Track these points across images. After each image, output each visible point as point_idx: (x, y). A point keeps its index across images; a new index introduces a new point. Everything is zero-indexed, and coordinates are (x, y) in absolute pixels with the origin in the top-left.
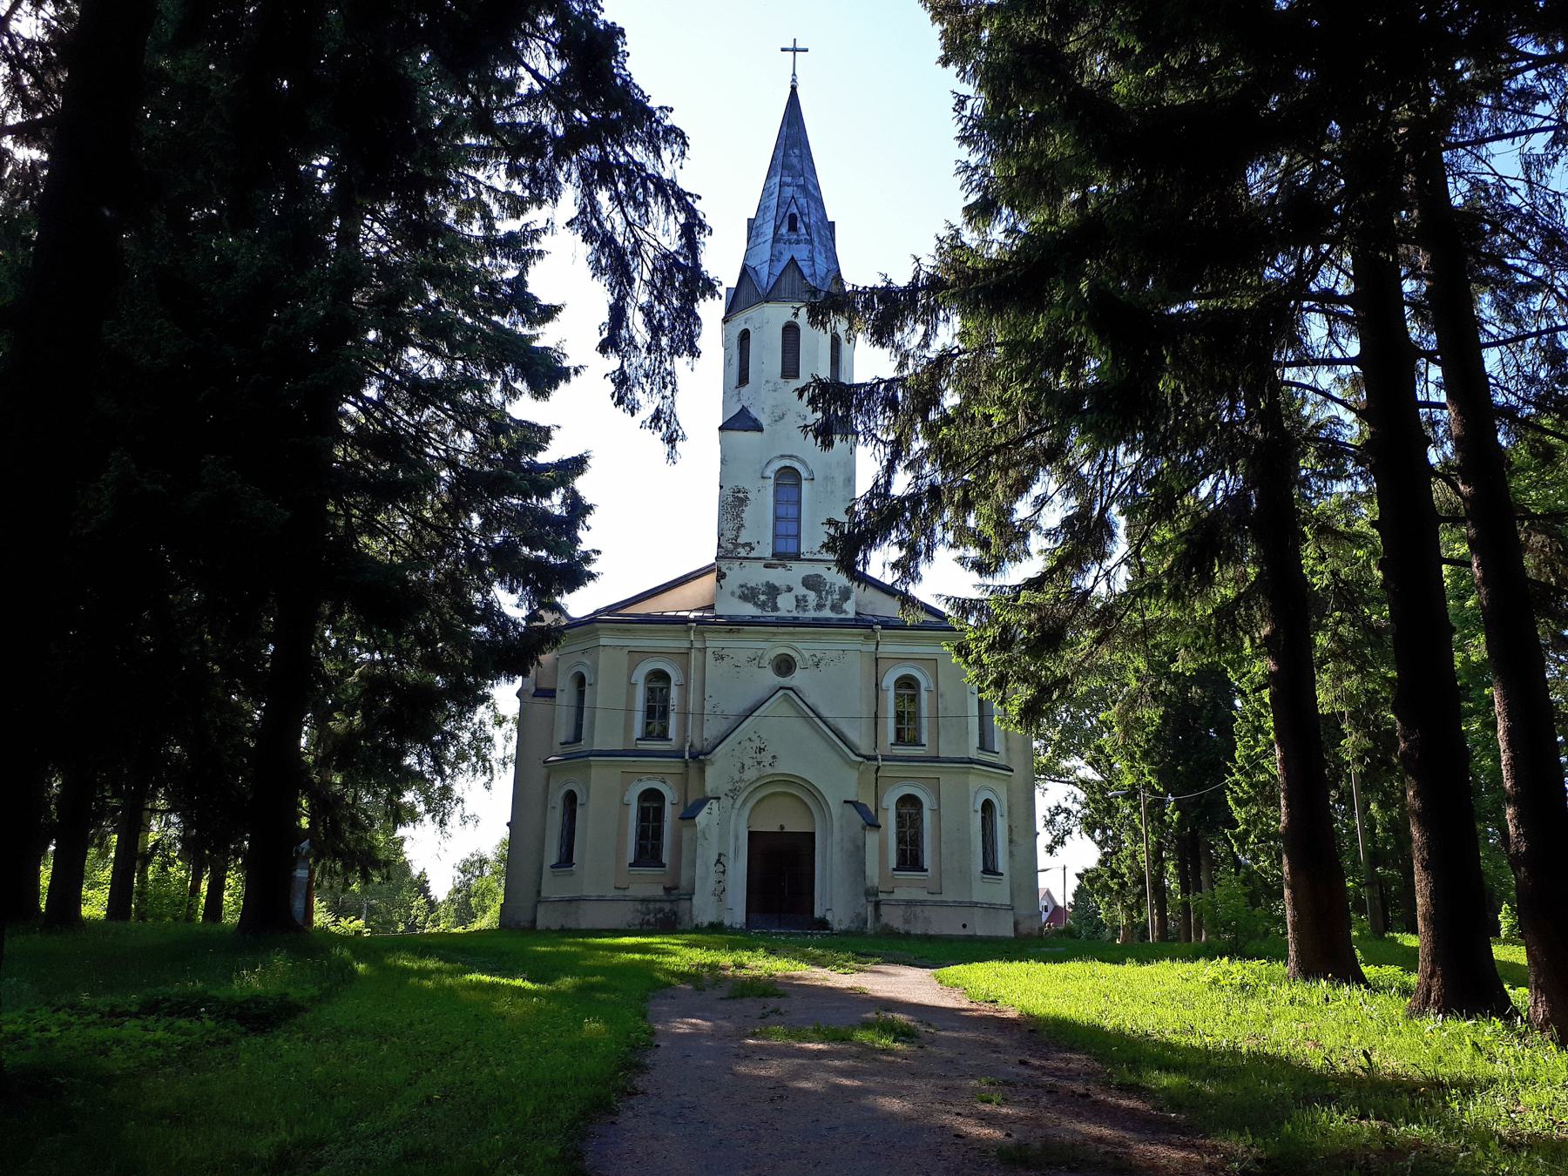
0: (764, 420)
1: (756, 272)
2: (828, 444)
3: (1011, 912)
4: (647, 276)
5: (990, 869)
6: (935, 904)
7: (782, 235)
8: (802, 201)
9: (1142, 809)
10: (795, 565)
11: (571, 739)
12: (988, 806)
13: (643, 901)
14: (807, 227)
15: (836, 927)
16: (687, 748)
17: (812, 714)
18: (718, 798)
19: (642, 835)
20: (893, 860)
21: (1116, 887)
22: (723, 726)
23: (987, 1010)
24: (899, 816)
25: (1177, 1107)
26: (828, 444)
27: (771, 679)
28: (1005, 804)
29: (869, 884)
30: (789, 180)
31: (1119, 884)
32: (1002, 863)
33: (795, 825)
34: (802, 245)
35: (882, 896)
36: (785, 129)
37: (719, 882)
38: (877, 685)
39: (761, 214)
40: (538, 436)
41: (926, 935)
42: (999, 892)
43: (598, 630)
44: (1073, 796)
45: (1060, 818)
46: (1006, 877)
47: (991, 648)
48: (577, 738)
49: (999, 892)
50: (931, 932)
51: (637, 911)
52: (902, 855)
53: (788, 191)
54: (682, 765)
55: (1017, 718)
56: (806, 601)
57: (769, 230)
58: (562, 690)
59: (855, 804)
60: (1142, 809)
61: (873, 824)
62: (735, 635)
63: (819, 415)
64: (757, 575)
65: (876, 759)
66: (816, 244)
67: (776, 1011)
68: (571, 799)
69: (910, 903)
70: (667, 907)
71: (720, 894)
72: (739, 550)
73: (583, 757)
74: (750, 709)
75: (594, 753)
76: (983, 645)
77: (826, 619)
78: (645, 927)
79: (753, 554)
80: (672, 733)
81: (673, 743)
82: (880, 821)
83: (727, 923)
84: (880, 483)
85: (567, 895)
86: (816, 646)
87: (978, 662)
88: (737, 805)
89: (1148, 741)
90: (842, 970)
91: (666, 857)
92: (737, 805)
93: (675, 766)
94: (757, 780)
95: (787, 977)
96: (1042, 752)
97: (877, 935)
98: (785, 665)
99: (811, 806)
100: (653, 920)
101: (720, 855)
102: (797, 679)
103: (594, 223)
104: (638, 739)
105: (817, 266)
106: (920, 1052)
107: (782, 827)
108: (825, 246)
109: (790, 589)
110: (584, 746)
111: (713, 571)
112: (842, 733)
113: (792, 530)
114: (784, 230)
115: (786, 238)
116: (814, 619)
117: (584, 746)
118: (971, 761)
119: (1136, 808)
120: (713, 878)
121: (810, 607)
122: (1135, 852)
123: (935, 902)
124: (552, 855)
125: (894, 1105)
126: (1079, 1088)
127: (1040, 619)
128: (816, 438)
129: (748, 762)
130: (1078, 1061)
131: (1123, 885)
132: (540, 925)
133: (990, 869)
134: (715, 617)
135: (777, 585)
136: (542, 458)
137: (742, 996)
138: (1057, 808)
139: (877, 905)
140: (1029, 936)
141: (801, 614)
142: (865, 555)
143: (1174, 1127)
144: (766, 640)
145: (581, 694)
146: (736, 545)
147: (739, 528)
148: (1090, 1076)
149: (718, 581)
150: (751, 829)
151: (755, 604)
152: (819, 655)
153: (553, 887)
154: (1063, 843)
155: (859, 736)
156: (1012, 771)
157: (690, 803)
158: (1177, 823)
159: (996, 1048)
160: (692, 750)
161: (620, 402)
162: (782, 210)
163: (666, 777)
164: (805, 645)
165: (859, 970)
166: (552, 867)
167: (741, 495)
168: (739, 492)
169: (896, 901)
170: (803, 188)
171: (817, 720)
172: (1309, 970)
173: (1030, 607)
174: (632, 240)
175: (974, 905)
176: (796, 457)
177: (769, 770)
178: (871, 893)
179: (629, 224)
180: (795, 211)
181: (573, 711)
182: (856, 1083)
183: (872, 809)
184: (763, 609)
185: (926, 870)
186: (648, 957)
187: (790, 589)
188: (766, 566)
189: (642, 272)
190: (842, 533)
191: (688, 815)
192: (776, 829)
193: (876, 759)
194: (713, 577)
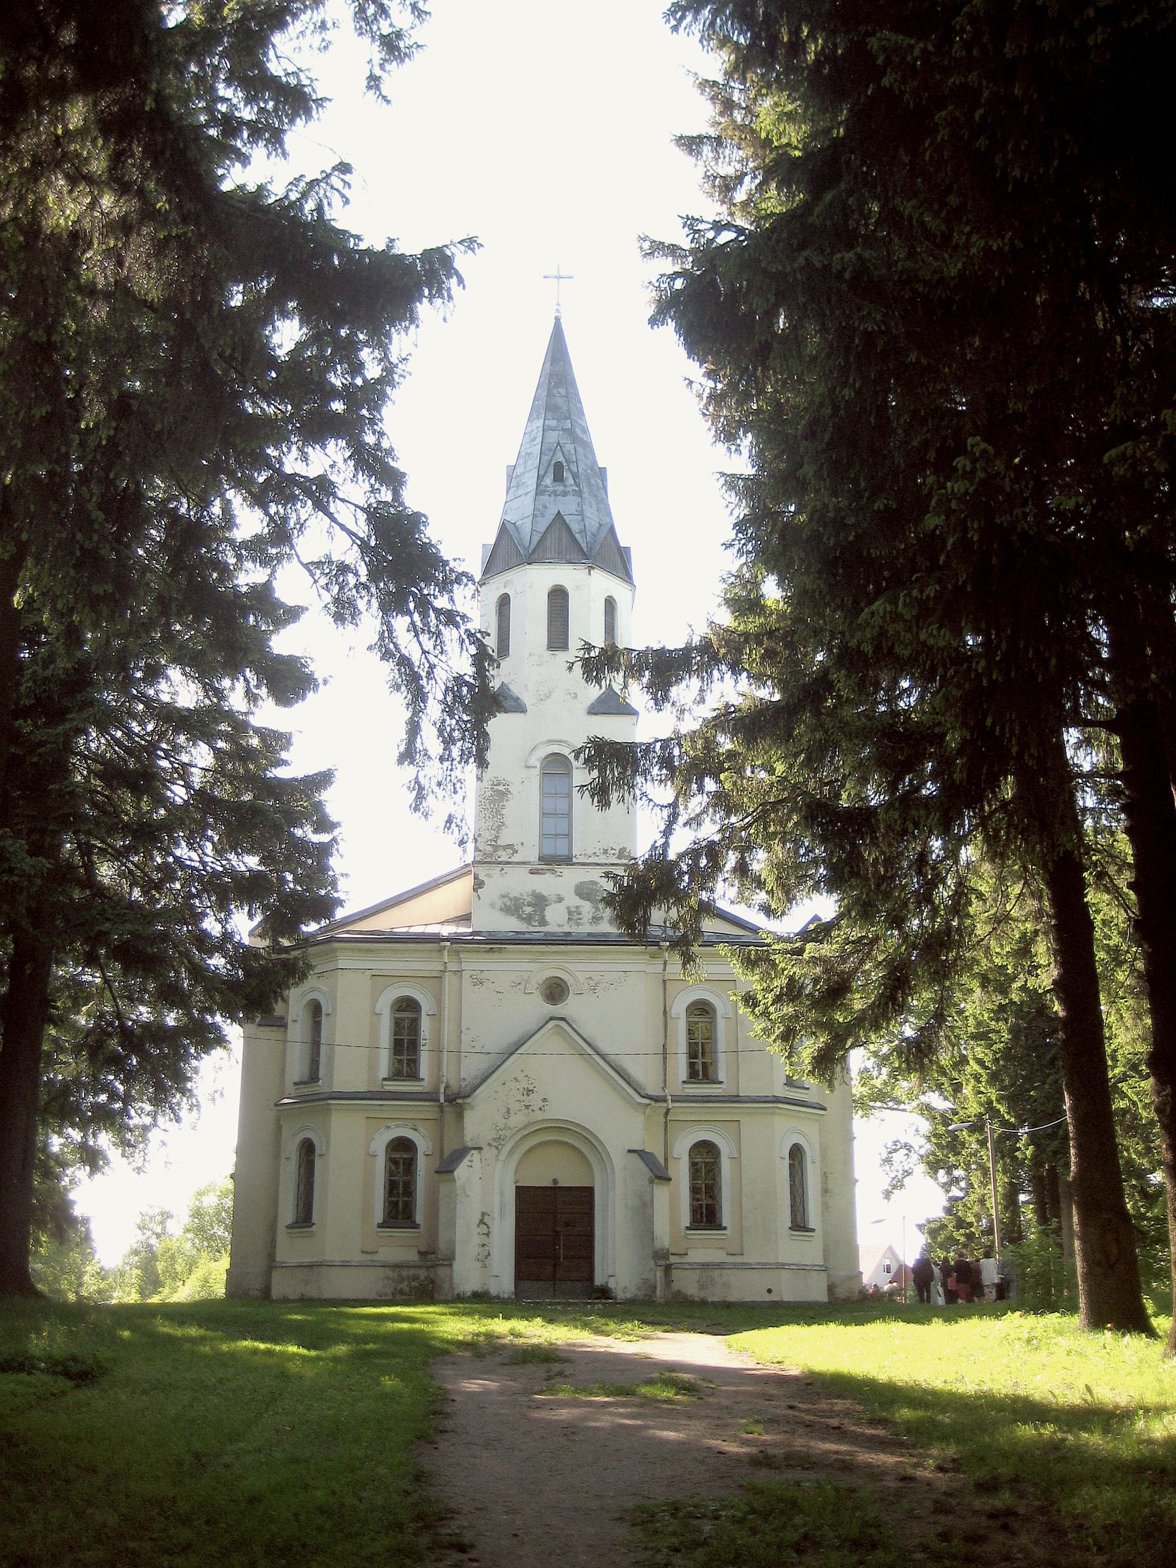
0: (527, 699)
1: (516, 528)
2: (605, 803)
3: (824, 1274)
4: (441, 697)
5: (799, 1225)
6: (736, 1266)
7: (547, 486)
8: (569, 447)
9: (989, 1145)
10: (566, 871)
11: (305, 1079)
12: (796, 1153)
13: (397, 1266)
14: (575, 476)
15: (620, 1295)
16: (442, 1090)
17: (590, 1051)
18: (479, 1149)
19: (391, 1187)
20: (686, 1218)
21: (962, 1239)
22: (483, 1063)
23: (773, 1369)
24: (693, 1165)
25: (909, 1431)
26: (605, 803)
27: (540, 1007)
28: (817, 1147)
29: (658, 1244)
30: (553, 423)
31: (966, 1235)
32: (814, 1220)
33: (570, 1178)
34: (570, 498)
35: (673, 1259)
36: (548, 365)
37: (484, 1245)
38: (665, 1012)
39: (522, 461)
40: (275, 741)
41: (725, 1302)
42: (808, 1251)
43: (335, 950)
44: (914, 1128)
45: (899, 1156)
46: (818, 1233)
47: (778, 1000)
48: (314, 1077)
49: (808, 1251)
50: (731, 1299)
51: (388, 1278)
52: (695, 1211)
53: (553, 437)
54: (438, 1109)
55: (809, 1068)
56: (580, 914)
57: (531, 481)
58: (295, 1021)
59: (641, 1154)
60: (989, 1145)
61: (661, 1176)
62: (496, 955)
63: (595, 773)
64: (521, 883)
65: (665, 1101)
66: (586, 495)
67: (560, 1374)
68: (308, 1148)
69: (705, 1266)
70: (422, 1273)
71: (484, 1259)
72: (499, 853)
73: (324, 1099)
74: (515, 1043)
75: (334, 1095)
76: (770, 997)
77: (604, 934)
78: (398, 1297)
79: (515, 859)
80: (424, 1070)
81: (424, 1083)
82: (671, 1173)
83: (493, 1292)
84: (657, 844)
85: (306, 1260)
86: (591, 967)
87: (766, 1014)
88: (503, 1156)
89: (996, 1061)
90: (626, 1338)
91: (419, 1217)
92: (503, 1156)
93: (427, 1110)
94: (525, 1127)
95: (568, 1345)
96: (875, 1073)
97: (667, 1303)
98: (555, 991)
99: (583, 1150)
100: (407, 1289)
101: (483, 1214)
102: (570, 1007)
103: (391, 646)
104: (384, 1079)
105: (587, 521)
106: (699, 1402)
107: (555, 1181)
108: (595, 496)
109: (560, 899)
110: (322, 1086)
111: (468, 873)
112: (624, 1070)
113: (562, 828)
114: (548, 481)
115: (551, 489)
116: (589, 934)
117: (322, 1086)
118: (777, 1100)
119: (982, 1143)
120: (477, 1240)
121: (585, 920)
122: (984, 1196)
123: (735, 1264)
124: (287, 1213)
125: (670, 1435)
126: (834, 1422)
127: (826, 971)
128: (592, 797)
129: (515, 1106)
130: (840, 1404)
131: (970, 1237)
132: (276, 1292)
133: (799, 1225)
134: (472, 934)
135: (545, 894)
136: (281, 773)
137: (525, 1362)
138: (895, 1143)
139: (668, 1268)
140: (846, 1301)
141: (574, 929)
142: (645, 912)
143: (902, 1445)
144: (532, 961)
145: (316, 1025)
146: (496, 848)
147: (499, 827)
148: (847, 1414)
149: (475, 890)
150: (518, 1184)
151: (520, 917)
152: (596, 977)
153: (290, 1250)
154: (902, 1186)
155: (645, 1073)
156: (824, 1109)
157: (446, 1154)
158: (1031, 1160)
159: (770, 1398)
160: (449, 1093)
161: (416, 809)
162: (546, 458)
163: (417, 1123)
164: (580, 966)
165: (645, 1338)
166: (288, 1227)
167: (501, 788)
168: (498, 785)
169: (690, 1264)
170: (570, 433)
171: (597, 1057)
172: (1097, 1322)
173: (814, 961)
174: (427, 665)
175: (780, 1266)
176: (565, 742)
177: (540, 1116)
178: (660, 1256)
179: (424, 652)
180: (561, 459)
181: (307, 1048)
182: (639, 1422)
183: (662, 1162)
184: (529, 924)
185: (725, 1228)
186: (417, 1326)
187: (560, 899)
188: (532, 872)
189: (435, 691)
190: (621, 886)
191: (446, 1167)
192: (547, 1183)
193: (665, 1101)
194: (469, 881)
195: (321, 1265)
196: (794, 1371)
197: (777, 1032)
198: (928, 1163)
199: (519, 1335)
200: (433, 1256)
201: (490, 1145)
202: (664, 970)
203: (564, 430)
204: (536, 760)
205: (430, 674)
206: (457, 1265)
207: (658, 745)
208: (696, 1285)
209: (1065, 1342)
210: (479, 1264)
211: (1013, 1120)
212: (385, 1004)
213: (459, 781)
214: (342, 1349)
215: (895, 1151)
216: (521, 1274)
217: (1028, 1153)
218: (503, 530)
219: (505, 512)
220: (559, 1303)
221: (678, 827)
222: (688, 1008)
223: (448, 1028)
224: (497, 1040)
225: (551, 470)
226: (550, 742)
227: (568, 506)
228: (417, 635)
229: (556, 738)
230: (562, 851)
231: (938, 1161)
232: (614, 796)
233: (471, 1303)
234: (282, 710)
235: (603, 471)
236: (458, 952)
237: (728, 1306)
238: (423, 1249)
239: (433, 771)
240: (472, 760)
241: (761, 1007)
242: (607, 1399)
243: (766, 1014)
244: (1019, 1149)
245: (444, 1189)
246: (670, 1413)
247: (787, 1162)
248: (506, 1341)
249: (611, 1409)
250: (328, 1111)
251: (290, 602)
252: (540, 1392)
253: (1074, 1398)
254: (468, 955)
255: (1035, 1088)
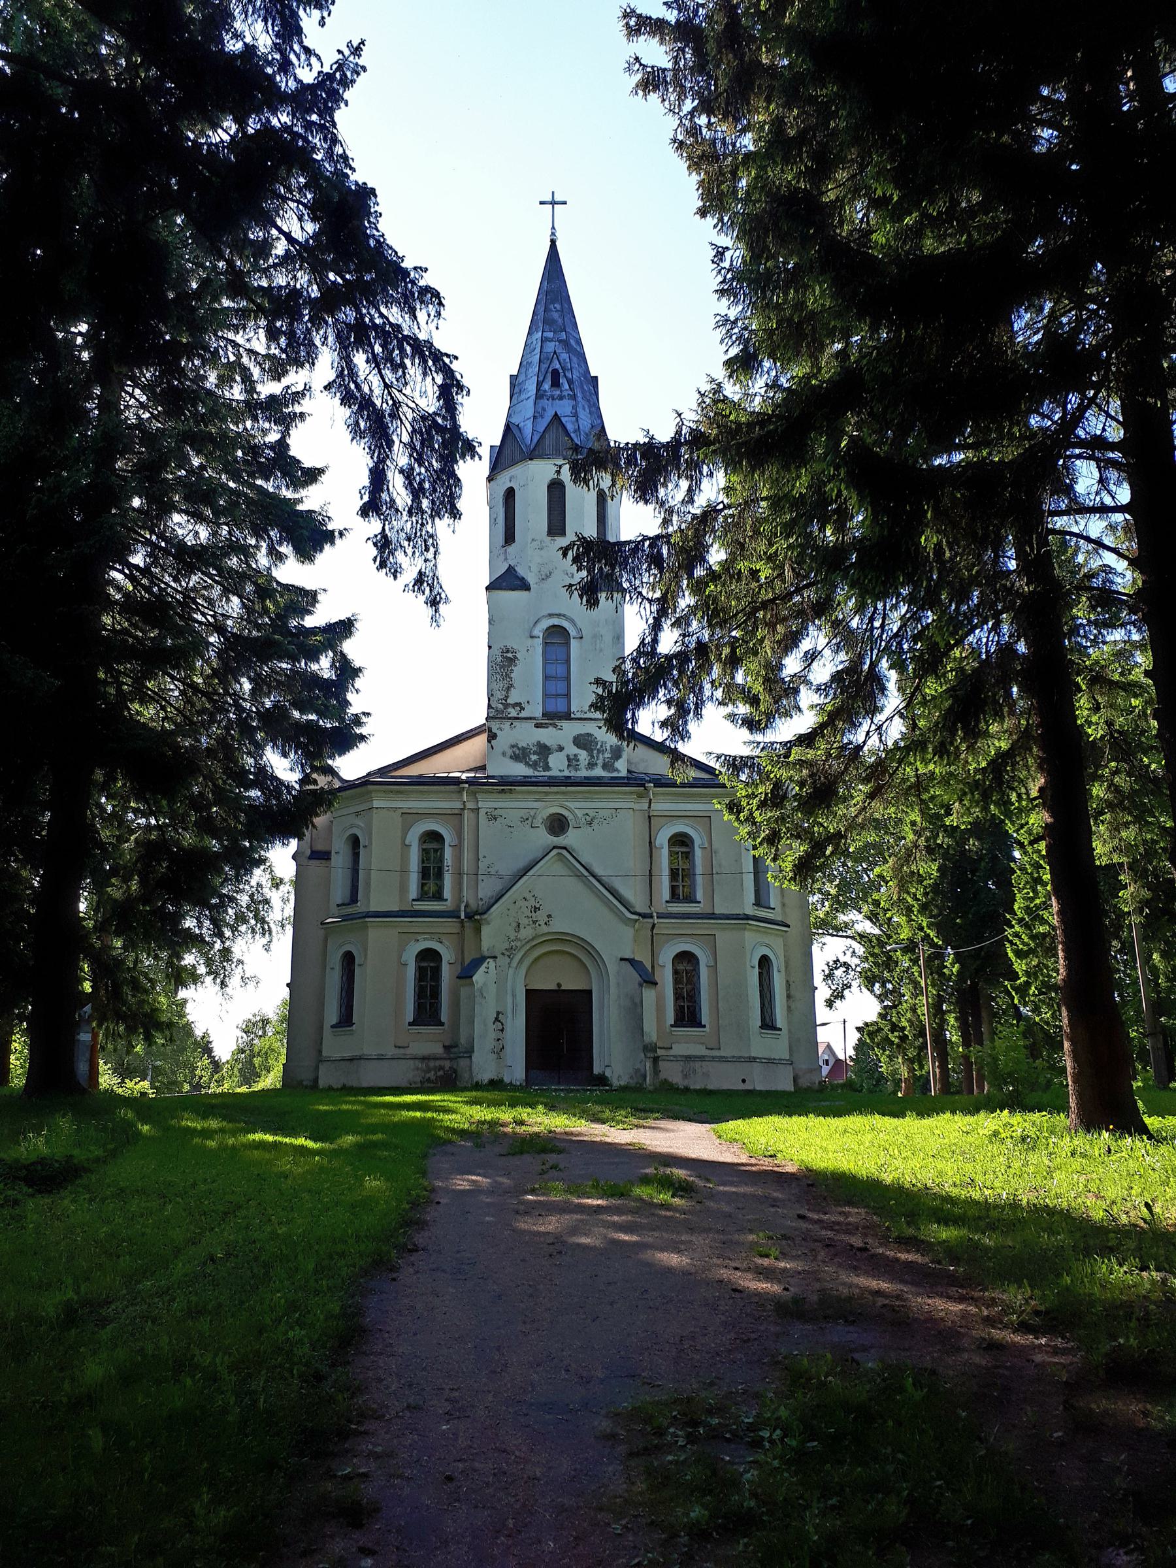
0: (531, 579)
2: (593, 603)
3: (790, 1068)
5: (768, 1024)
6: (713, 1059)
7: (545, 391)
8: (564, 356)
10: (565, 724)
11: (347, 901)
13: (424, 1059)
14: (570, 382)
15: (616, 1083)
17: (586, 874)
20: (670, 1018)
21: (897, 1041)
23: (767, 1164)
24: (676, 972)
25: (955, 1259)
26: (593, 603)
28: (782, 959)
29: (647, 1039)
30: (550, 335)
31: (900, 1037)
33: (571, 983)
34: (566, 402)
35: (660, 1052)
37: (498, 1040)
38: (650, 842)
39: (523, 370)
40: (305, 599)
42: (778, 1046)
44: (851, 950)
45: (839, 973)
47: (762, 805)
48: (354, 899)
49: (778, 1046)
50: (710, 1087)
51: (418, 1069)
53: (550, 347)
54: (458, 925)
55: (791, 874)
56: (578, 760)
57: (531, 387)
59: (631, 961)
63: (584, 573)
64: (527, 735)
65: (652, 917)
66: (579, 399)
68: (349, 960)
69: (688, 1058)
70: (447, 1064)
71: (499, 1051)
75: (370, 914)
77: (598, 778)
78: (426, 1085)
79: (523, 714)
80: (447, 894)
81: (448, 903)
82: (657, 979)
84: (646, 641)
85: (348, 1054)
87: (750, 819)
89: (926, 894)
90: (621, 1126)
93: (451, 925)
94: (533, 939)
97: (656, 1091)
98: (558, 825)
100: (433, 1078)
101: (498, 1013)
102: (570, 838)
103: (352, 386)
104: (413, 900)
105: (581, 422)
106: (698, 1207)
107: (559, 985)
109: (561, 749)
110: (360, 907)
112: (616, 890)
113: (561, 687)
114: (547, 386)
116: (586, 778)
118: (747, 917)
119: (915, 961)
120: (492, 1035)
122: (915, 1005)
123: (713, 1057)
124: (332, 1015)
126: (857, 1241)
128: (581, 597)
129: (524, 921)
130: (856, 1215)
131: (904, 1038)
133: (768, 1024)
134: (485, 778)
135: (548, 744)
139: (656, 1060)
140: (808, 1090)
141: (573, 774)
143: (953, 1280)
145: (356, 856)
146: (506, 706)
147: (508, 689)
148: (868, 1229)
149: (489, 741)
151: (527, 764)
153: (335, 1046)
156: (788, 926)
161: (382, 565)
162: (544, 366)
163: (440, 936)
164: (578, 805)
166: (332, 1027)
167: (510, 655)
168: (508, 652)
171: (591, 878)
172: (1091, 1121)
173: (801, 763)
175: (753, 1060)
176: (564, 616)
177: (545, 929)
178: (650, 1048)
179: (386, 386)
180: (558, 366)
181: (349, 873)
182: (635, 1238)
184: (535, 769)
185: (704, 1026)
186: (429, 1115)
187: (561, 749)
188: (537, 726)
189: (402, 434)
191: (466, 973)
193: (652, 917)
195: (360, 1058)
196: (791, 1168)
197: (763, 835)
198: (866, 978)
199: (522, 1123)
200: (455, 1050)
201: (503, 954)
202: (649, 807)
203: (560, 341)
204: (538, 631)
205: (394, 415)
206: (476, 1057)
207: (647, 543)
208: (680, 1074)
209: (1066, 1144)
210: (495, 1056)
211: (940, 943)
212: (413, 837)
213: (431, 536)
214: (349, 1139)
215: (836, 968)
216: (531, 1064)
217: (954, 970)
218: (508, 429)
219: (509, 415)
220: (562, 1090)
221: (666, 624)
222: (669, 841)
223: (467, 856)
224: (508, 867)
225: (549, 376)
226: (551, 615)
227: (564, 408)
228: (377, 366)
229: (557, 612)
230: (561, 707)
231: (875, 977)
232: (602, 596)
233: (488, 1091)
234: (307, 567)
235: (595, 379)
236: (475, 793)
237: (707, 1093)
238: (447, 1044)
239: (403, 523)
240: (260, 20)
241: (746, 813)
242: (599, 1202)
243: (750, 819)
244: (946, 967)
245: (464, 992)
246: (668, 1224)
247: (757, 970)
248: (509, 1129)
249: (604, 1217)
250: (365, 927)
251: (307, 464)
252: (533, 1192)
253: (1130, 1215)
254: (484, 795)
255: (959, 917)
